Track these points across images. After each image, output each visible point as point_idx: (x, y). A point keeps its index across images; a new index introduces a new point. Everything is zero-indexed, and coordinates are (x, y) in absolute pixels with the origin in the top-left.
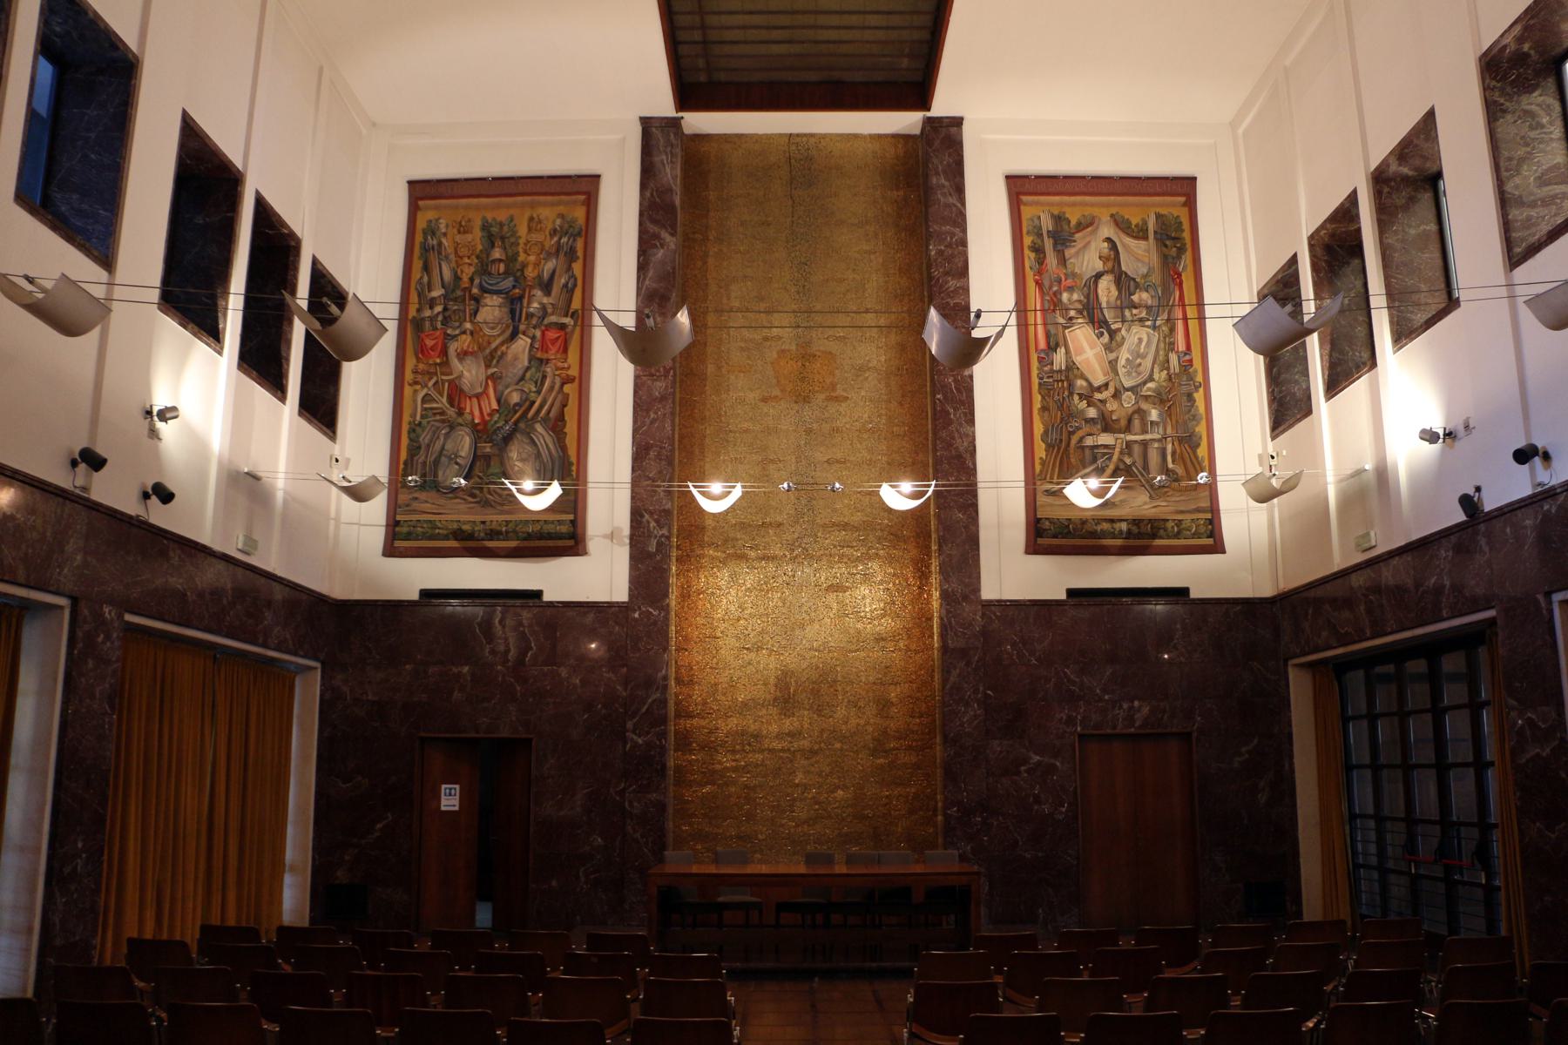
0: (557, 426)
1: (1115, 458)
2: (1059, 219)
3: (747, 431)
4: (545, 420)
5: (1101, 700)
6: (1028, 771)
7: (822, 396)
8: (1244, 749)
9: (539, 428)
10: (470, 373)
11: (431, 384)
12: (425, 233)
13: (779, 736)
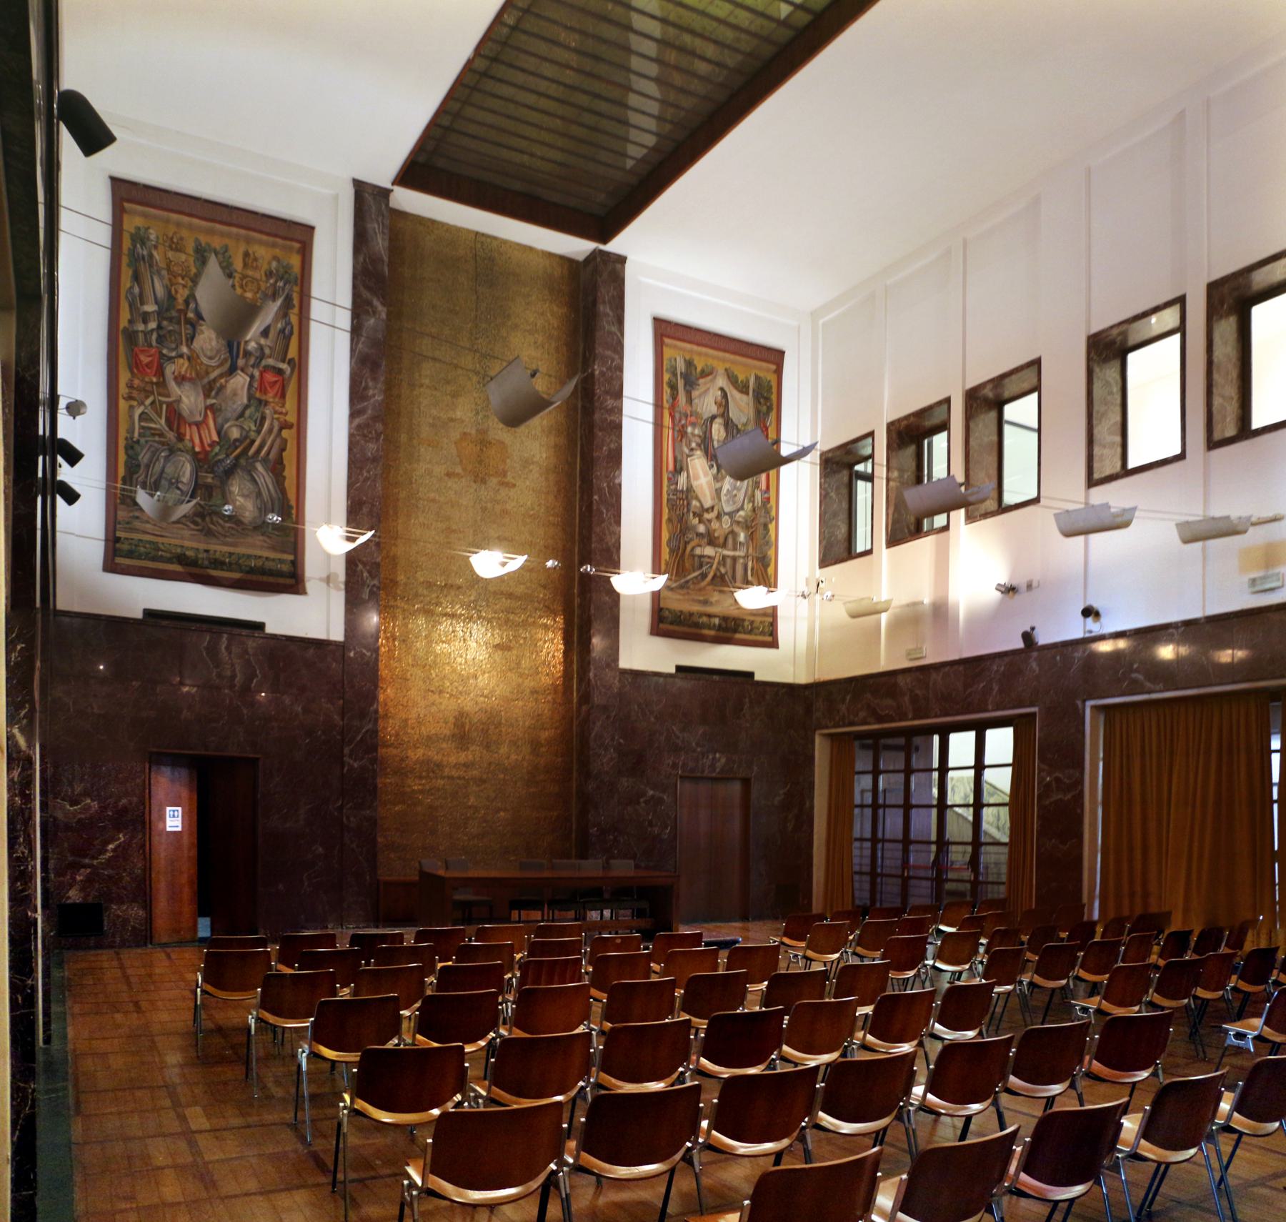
0: (277, 468)
3: (433, 500)
4: (265, 461)
5: (694, 751)
6: (645, 802)
9: (259, 467)
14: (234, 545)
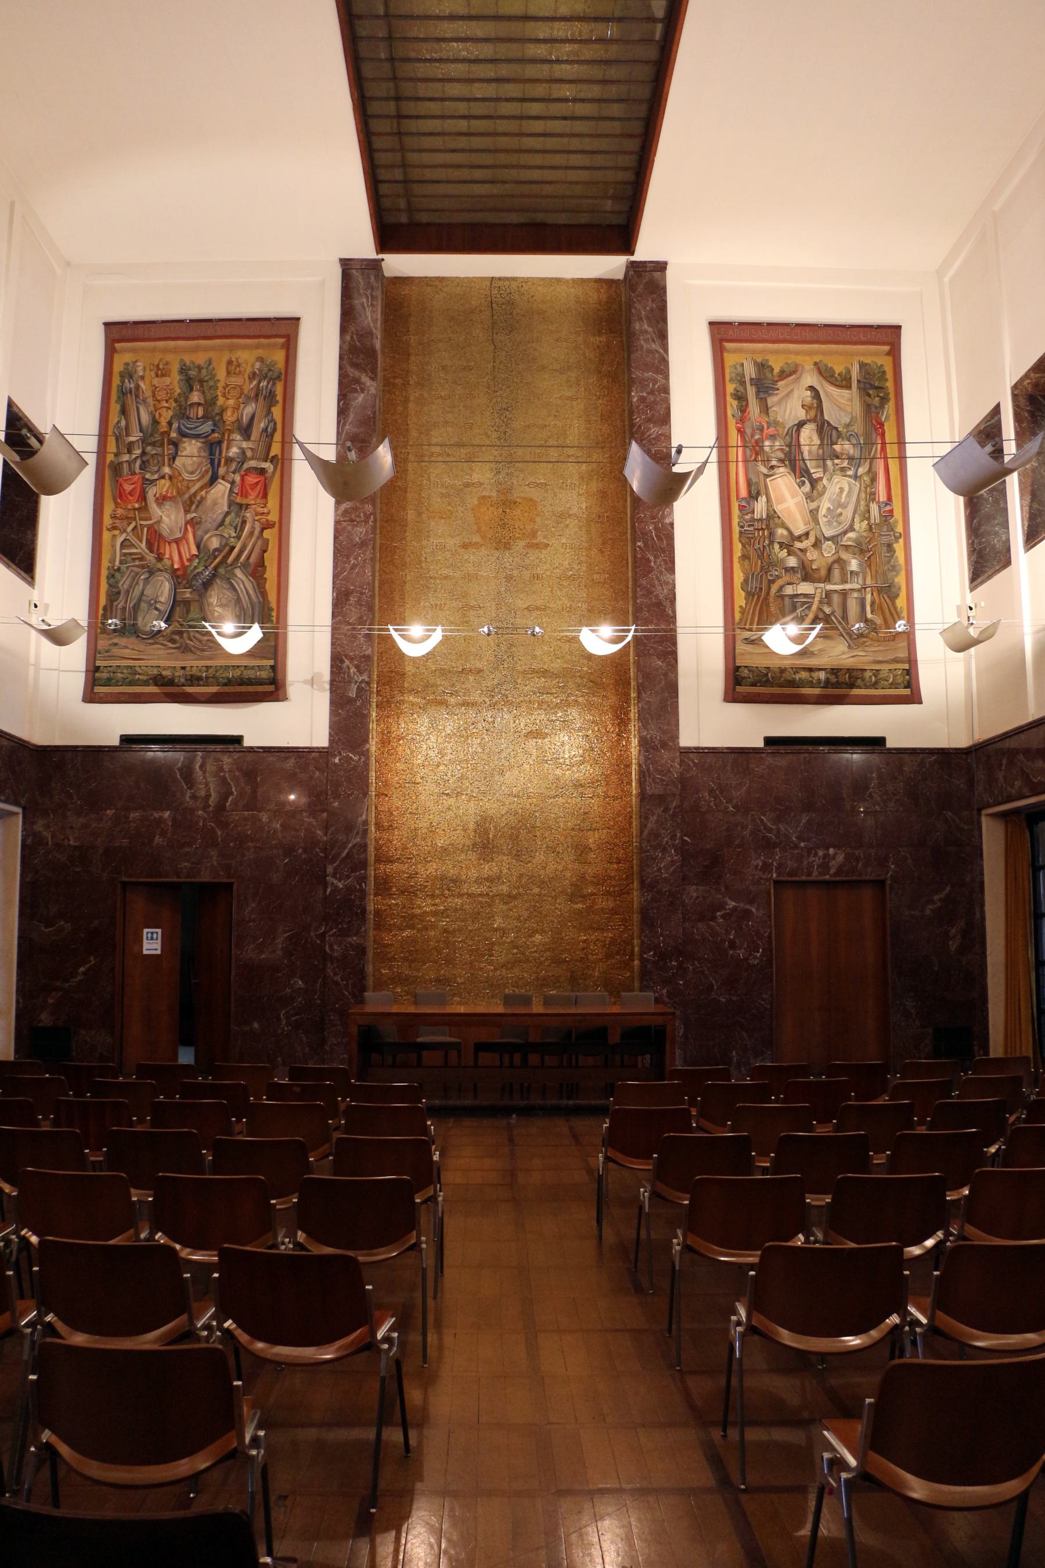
0: (257, 572)
1: (814, 607)
2: (762, 367)
3: (446, 577)
4: (245, 566)
5: (796, 846)
6: (723, 917)
7: (522, 543)
8: (936, 897)
9: (238, 573)
10: (170, 519)
11: (129, 529)
12: (122, 376)
13: (479, 881)
14: (210, 658)
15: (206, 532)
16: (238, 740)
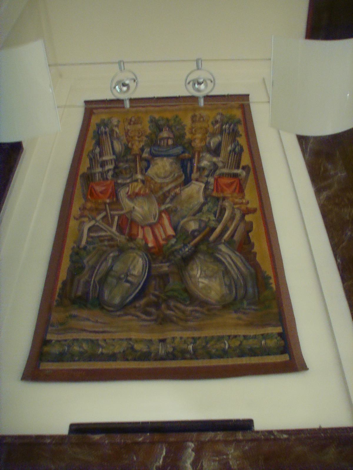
4: (230, 243)
9: (223, 248)
10: (142, 209)
11: (99, 218)
15: (184, 217)
16: (246, 425)
